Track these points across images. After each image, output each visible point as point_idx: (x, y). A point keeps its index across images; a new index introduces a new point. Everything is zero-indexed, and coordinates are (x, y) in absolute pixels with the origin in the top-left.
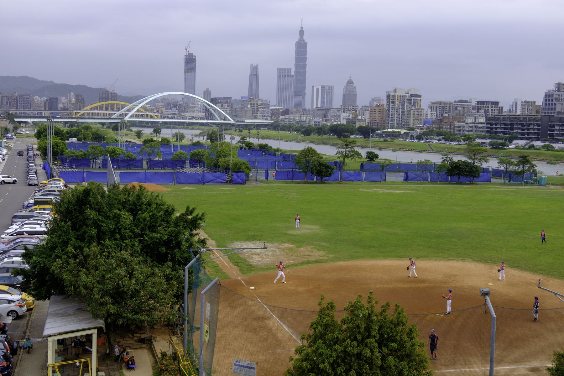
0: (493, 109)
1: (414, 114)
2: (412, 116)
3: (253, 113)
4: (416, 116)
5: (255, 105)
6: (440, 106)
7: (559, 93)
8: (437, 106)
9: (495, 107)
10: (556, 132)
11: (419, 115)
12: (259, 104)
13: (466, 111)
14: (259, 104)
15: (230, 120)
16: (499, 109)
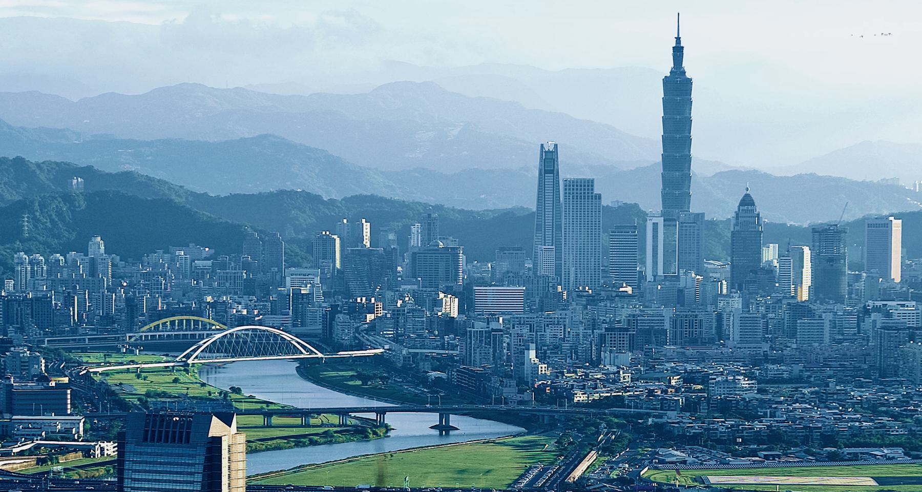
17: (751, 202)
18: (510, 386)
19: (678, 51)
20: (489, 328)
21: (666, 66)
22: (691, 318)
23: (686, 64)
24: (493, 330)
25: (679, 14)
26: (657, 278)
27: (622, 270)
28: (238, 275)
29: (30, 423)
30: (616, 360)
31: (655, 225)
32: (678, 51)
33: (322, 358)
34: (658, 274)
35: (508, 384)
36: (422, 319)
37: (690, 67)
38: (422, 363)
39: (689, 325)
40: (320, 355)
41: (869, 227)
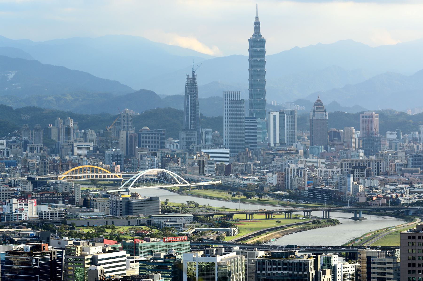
0: (362, 171)
1: (297, 181)
2: (296, 181)
3: (200, 171)
4: (299, 182)
5: (202, 162)
6: (348, 163)
7: (343, 176)
8: (345, 163)
9: (363, 170)
10: (325, 196)
11: (300, 181)
12: (205, 161)
13: (318, 181)
14: (205, 161)
15: (186, 183)
16: (366, 171)
17: (321, 103)
18: (362, 196)
19: (257, 25)
20: (297, 167)
21: (250, 33)
22: (378, 162)
23: (262, 31)
24: (300, 168)
25: (257, 4)
26: (276, 145)
27: (249, 141)
28: (40, 147)
29: (168, 219)
30: (371, 184)
31: (275, 116)
32: (257, 25)
33: (190, 186)
34: (277, 143)
35: (361, 195)
36: (213, 166)
37: (264, 33)
38: (265, 187)
39: (368, 166)
40: (188, 184)
41: (362, 118)
